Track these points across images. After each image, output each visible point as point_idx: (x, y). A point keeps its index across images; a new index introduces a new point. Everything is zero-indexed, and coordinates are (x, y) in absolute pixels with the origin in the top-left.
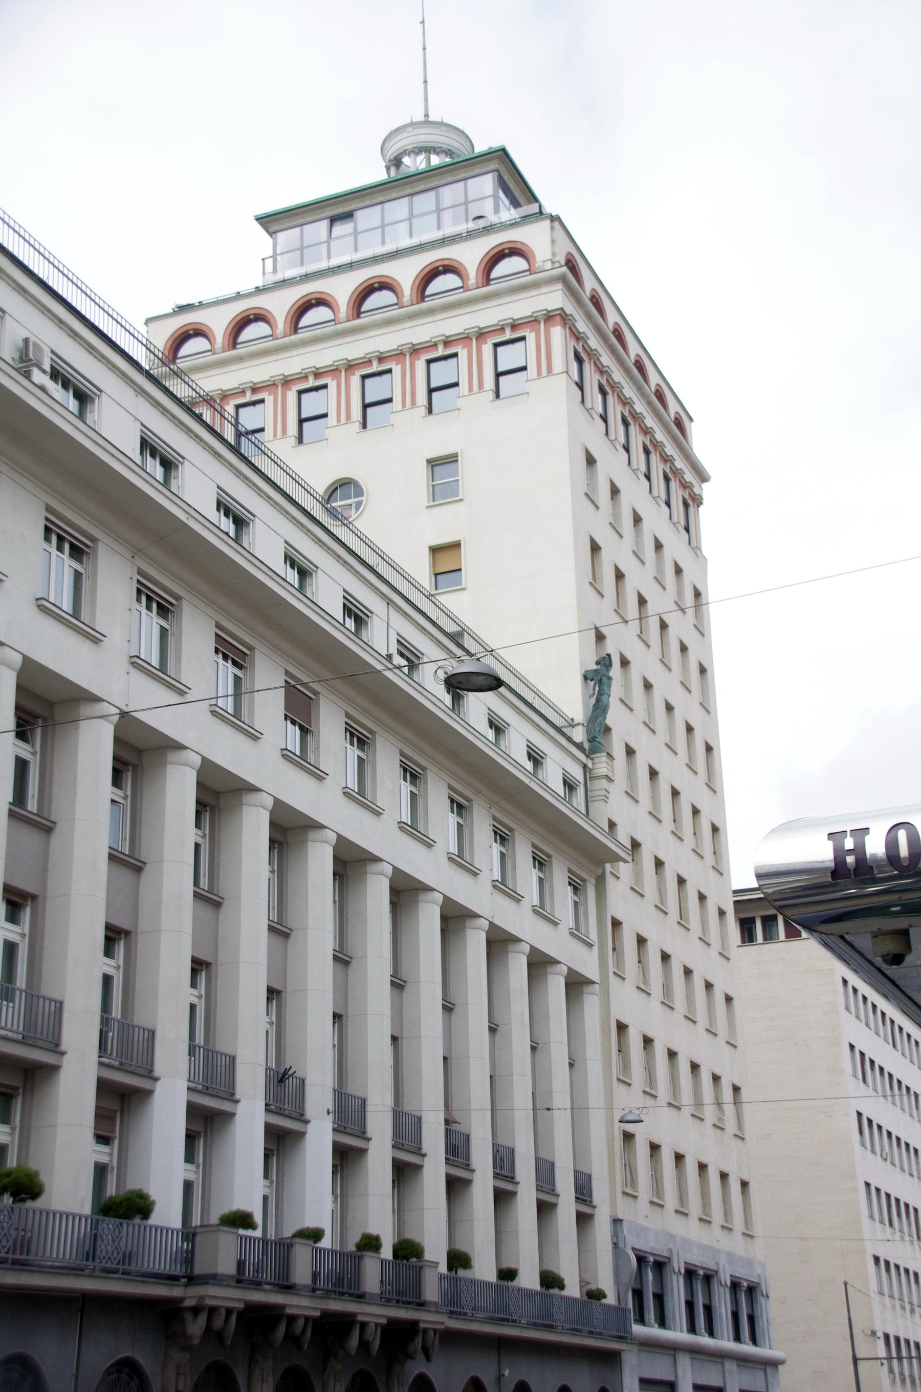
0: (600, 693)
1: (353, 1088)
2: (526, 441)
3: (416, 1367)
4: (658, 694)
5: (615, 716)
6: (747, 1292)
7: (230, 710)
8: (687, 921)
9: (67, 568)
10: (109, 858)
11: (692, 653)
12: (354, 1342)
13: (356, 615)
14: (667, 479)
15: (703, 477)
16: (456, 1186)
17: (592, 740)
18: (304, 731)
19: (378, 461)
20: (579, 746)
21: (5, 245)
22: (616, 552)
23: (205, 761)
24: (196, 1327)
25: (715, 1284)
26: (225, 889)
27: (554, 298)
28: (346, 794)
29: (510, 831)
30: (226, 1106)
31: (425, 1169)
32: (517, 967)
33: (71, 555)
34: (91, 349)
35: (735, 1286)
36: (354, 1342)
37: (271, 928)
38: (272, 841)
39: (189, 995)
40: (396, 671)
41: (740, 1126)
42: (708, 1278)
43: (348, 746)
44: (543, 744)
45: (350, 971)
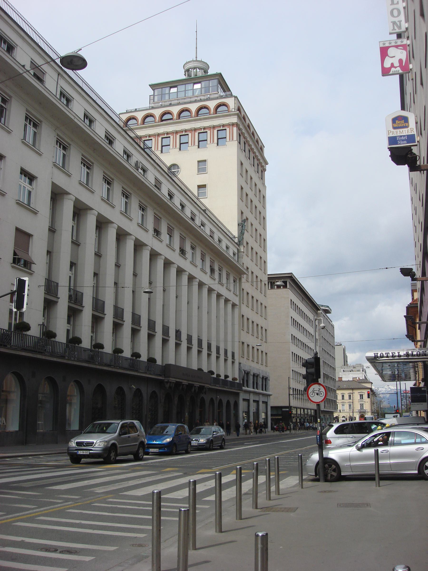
0: (242, 229)
1: (137, 312)
2: (225, 158)
3: (202, 395)
4: (254, 227)
5: (247, 236)
6: (265, 379)
9: (31, 130)
10: (49, 230)
12: (193, 390)
13: (171, 196)
14: (245, 143)
15: (267, 163)
16: (151, 337)
17: (239, 242)
18: (170, 236)
19: (184, 161)
20: (236, 243)
21: (2, 7)
22: (247, 189)
23: (76, 199)
24: (167, 386)
26: (81, 240)
27: (235, 120)
28: (102, 199)
29: (40, 122)
31: (182, 345)
32: (185, 279)
33: (33, 126)
35: (263, 378)
36: (193, 390)
37: (95, 254)
38: (97, 226)
39: (70, 273)
40: (27, 73)
41: (266, 340)
42: (257, 376)
43: (104, 183)
44: (222, 237)
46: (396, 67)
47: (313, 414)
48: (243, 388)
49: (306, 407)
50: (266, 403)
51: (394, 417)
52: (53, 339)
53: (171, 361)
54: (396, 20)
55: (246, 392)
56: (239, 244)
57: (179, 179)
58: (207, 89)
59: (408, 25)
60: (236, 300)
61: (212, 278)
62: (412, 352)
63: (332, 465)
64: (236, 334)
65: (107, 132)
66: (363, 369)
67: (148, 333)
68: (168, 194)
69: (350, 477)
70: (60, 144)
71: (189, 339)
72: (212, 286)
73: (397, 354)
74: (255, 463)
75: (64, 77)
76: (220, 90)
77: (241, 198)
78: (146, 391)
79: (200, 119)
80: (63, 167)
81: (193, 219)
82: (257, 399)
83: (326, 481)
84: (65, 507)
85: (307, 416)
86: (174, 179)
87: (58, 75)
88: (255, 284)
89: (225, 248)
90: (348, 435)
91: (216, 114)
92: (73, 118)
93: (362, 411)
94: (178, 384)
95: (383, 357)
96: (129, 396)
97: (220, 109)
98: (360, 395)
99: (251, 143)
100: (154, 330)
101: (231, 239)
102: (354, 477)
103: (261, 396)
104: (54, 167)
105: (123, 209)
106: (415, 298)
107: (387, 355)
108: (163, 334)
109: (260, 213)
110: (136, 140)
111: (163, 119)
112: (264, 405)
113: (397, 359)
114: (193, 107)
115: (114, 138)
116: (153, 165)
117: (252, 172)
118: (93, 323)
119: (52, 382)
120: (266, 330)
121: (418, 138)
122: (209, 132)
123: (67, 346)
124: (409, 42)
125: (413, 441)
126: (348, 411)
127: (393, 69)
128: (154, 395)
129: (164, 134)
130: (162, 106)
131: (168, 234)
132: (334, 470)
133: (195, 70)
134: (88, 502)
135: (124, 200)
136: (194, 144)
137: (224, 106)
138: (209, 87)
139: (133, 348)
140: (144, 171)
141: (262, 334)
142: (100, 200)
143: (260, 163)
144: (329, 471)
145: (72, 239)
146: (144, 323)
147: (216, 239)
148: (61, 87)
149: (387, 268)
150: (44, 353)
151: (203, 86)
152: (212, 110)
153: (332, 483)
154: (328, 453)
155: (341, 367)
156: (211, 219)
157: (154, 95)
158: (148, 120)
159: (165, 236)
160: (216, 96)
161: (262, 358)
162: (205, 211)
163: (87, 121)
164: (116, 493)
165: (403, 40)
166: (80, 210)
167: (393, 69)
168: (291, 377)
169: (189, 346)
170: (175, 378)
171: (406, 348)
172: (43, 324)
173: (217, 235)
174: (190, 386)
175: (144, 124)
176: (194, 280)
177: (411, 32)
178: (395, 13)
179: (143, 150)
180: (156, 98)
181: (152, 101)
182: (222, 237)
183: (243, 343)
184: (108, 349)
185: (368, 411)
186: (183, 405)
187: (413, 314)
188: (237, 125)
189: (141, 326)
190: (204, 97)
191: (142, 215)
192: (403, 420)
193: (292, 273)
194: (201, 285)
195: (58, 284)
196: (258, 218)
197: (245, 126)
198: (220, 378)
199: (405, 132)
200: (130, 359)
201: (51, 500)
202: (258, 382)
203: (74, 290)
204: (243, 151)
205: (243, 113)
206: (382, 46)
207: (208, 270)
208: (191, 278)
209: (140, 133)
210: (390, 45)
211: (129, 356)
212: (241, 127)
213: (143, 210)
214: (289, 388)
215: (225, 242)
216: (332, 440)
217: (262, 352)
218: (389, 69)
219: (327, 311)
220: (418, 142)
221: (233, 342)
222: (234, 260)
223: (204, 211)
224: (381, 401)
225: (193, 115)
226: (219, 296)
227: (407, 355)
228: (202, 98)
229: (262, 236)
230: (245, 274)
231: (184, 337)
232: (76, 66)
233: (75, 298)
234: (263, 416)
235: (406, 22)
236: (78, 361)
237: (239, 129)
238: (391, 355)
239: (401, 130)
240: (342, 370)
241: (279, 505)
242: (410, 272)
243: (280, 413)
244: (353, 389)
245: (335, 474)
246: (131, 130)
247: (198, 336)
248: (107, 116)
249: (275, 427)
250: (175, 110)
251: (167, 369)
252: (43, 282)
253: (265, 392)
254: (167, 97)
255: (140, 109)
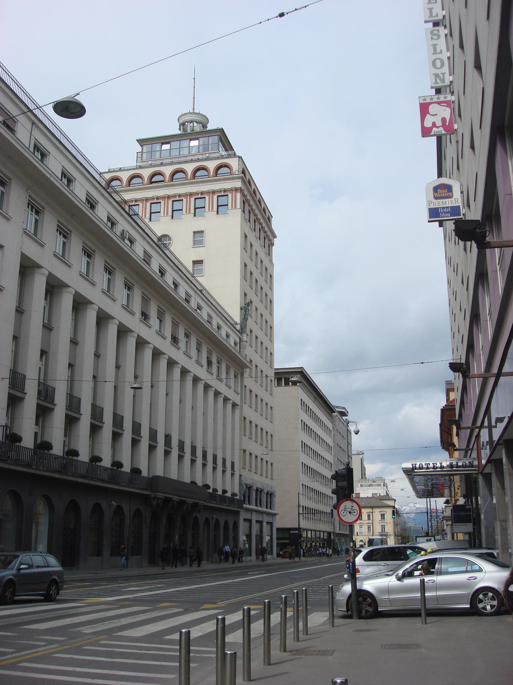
0: (246, 314)
1: (119, 412)
2: (226, 229)
5: (250, 323)
6: (270, 495)
7: (61, 254)
8: (252, 374)
11: (269, 297)
12: (185, 508)
13: (162, 272)
15: (275, 236)
16: (135, 442)
17: (242, 329)
18: (161, 321)
19: (177, 230)
20: (238, 331)
22: (251, 267)
23: (50, 273)
24: (154, 502)
25: (262, 493)
26: (54, 324)
27: (238, 184)
28: (81, 275)
29: (9, 180)
30: (120, 431)
32: (177, 373)
34: (135, 229)
35: (267, 493)
36: (185, 508)
38: (73, 308)
41: (272, 447)
42: (261, 491)
43: (83, 256)
44: (222, 323)
45: (77, 347)
46: (438, 127)
47: (326, 538)
48: (244, 505)
49: (318, 529)
50: (271, 524)
51: (427, 540)
52: (18, 444)
53: (159, 472)
54: (439, 72)
55: (248, 510)
56: (242, 331)
57: (171, 252)
58: (206, 148)
59: (454, 78)
60: (237, 399)
61: (209, 372)
62: (457, 463)
63: (487, 594)
64: (237, 440)
65: (88, 194)
66: (384, 483)
67: (132, 438)
68: (159, 270)
69: (390, 612)
70: (32, 207)
71: (181, 445)
72: (209, 382)
73: (439, 465)
74: (283, 596)
75: (39, 127)
76: (221, 148)
77: (244, 278)
78: (128, 509)
79: (197, 183)
80: (34, 235)
81: (187, 301)
82: (261, 519)
83: (360, 617)
84: (51, 651)
85: (319, 540)
86: (167, 252)
87: (33, 124)
88: (259, 380)
89: (224, 336)
90: (379, 562)
91: (216, 176)
92: (49, 176)
93: (383, 533)
94: (167, 501)
95: (422, 468)
96: (108, 514)
97: (221, 171)
98: (382, 514)
99: (257, 212)
100: (139, 435)
101: (232, 325)
102: (393, 612)
103: (265, 515)
104: (24, 235)
105: (105, 287)
106: (451, 399)
107: (427, 466)
108: (150, 439)
109: (266, 295)
110: (121, 204)
111: (153, 180)
112: (269, 526)
113: (438, 471)
114: (189, 168)
115: (97, 202)
116: (142, 235)
117: (257, 246)
118: (66, 424)
119: (16, 496)
120: (272, 436)
121: (464, 210)
122: (207, 198)
123: (35, 452)
124: (453, 98)
125: (464, 568)
126: (367, 534)
127: (435, 129)
128: (138, 514)
129: (154, 199)
130: (151, 166)
131: (158, 318)
132: (370, 605)
133: (192, 124)
134: (77, 645)
135: (106, 276)
136: (190, 212)
137: (203, 171)
138: (209, 144)
139: (113, 456)
140: (132, 242)
141: (267, 441)
142: (78, 276)
143: (268, 236)
144: (364, 606)
145: (43, 322)
146: (128, 426)
147: (215, 326)
148: (35, 139)
149: (422, 363)
150: (7, 461)
151: (201, 144)
152: (212, 172)
153: (368, 620)
154: (362, 584)
155: (359, 481)
156: (209, 301)
157: (142, 152)
158: (134, 181)
159: (154, 321)
160: (217, 155)
161: (267, 470)
162: (201, 292)
163: (65, 181)
164: (109, 633)
165: (446, 96)
166: (53, 287)
167: (435, 129)
168: (301, 493)
169: (181, 454)
170: (163, 493)
171: (443, 460)
172: (7, 426)
173: (216, 320)
174: (182, 503)
175: (129, 186)
176: (188, 374)
177: (458, 87)
178: (438, 64)
179: (130, 216)
180: (145, 156)
181: (139, 159)
182: (222, 323)
183: (245, 451)
184: (84, 456)
185: (391, 534)
186: (174, 528)
187: (449, 418)
188: (241, 190)
189: (124, 429)
190: (203, 157)
191: (128, 295)
192: (443, 544)
193: (302, 368)
194: (196, 380)
195: (25, 376)
196: (264, 301)
197: (250, 192)
198: (217, 493)
199: (448, 203)
200: (111, 469)
201: (31, 642)
202: (262, 498)
203: (45, 384)
204: (248, 222)
205: (248, 177)
206: (422, 102)
207: (205, 363)
208: (184, 372)
209: (127, 196)
210: (432, 101)
211: (109, 466)
212: (246, 192)
213: (129, 289)
214: (299, 506)
215: (225, 329)
216: (360, 568)
217: (267, 462)
218: (431, 128)
219: (343, 414)
220: (463, 214)
221: (233, 449)
222: (235, 350)
223: (201, 291)
224: (405, 522)
225: (189, 177)
226: (217, 393)
227: (451, 466)
228: (200, 157)
229: (268, 323)
230: (249, 367)
231: (175, 443)
232: (73, 113)
233: (46, 394)
234: (267, 538)
235: (450, 75)
236: (48, 471)
237: (244, 195)
238: (432, 466)
239: (444, 200)
240: (359, 484)
241: (311, 647)
242: (461, 368)
243: (287, 536)
244: (372, 507)
245: (370, 609)
246: (117, 192)
247: (192, 443)
248: (87, 174)
249: (281, 553)
250: (168, 171)
251: (154, 482)
252: (7, 374)
253: (269, 511)
254: (158, 155)
255: (126, 168)
